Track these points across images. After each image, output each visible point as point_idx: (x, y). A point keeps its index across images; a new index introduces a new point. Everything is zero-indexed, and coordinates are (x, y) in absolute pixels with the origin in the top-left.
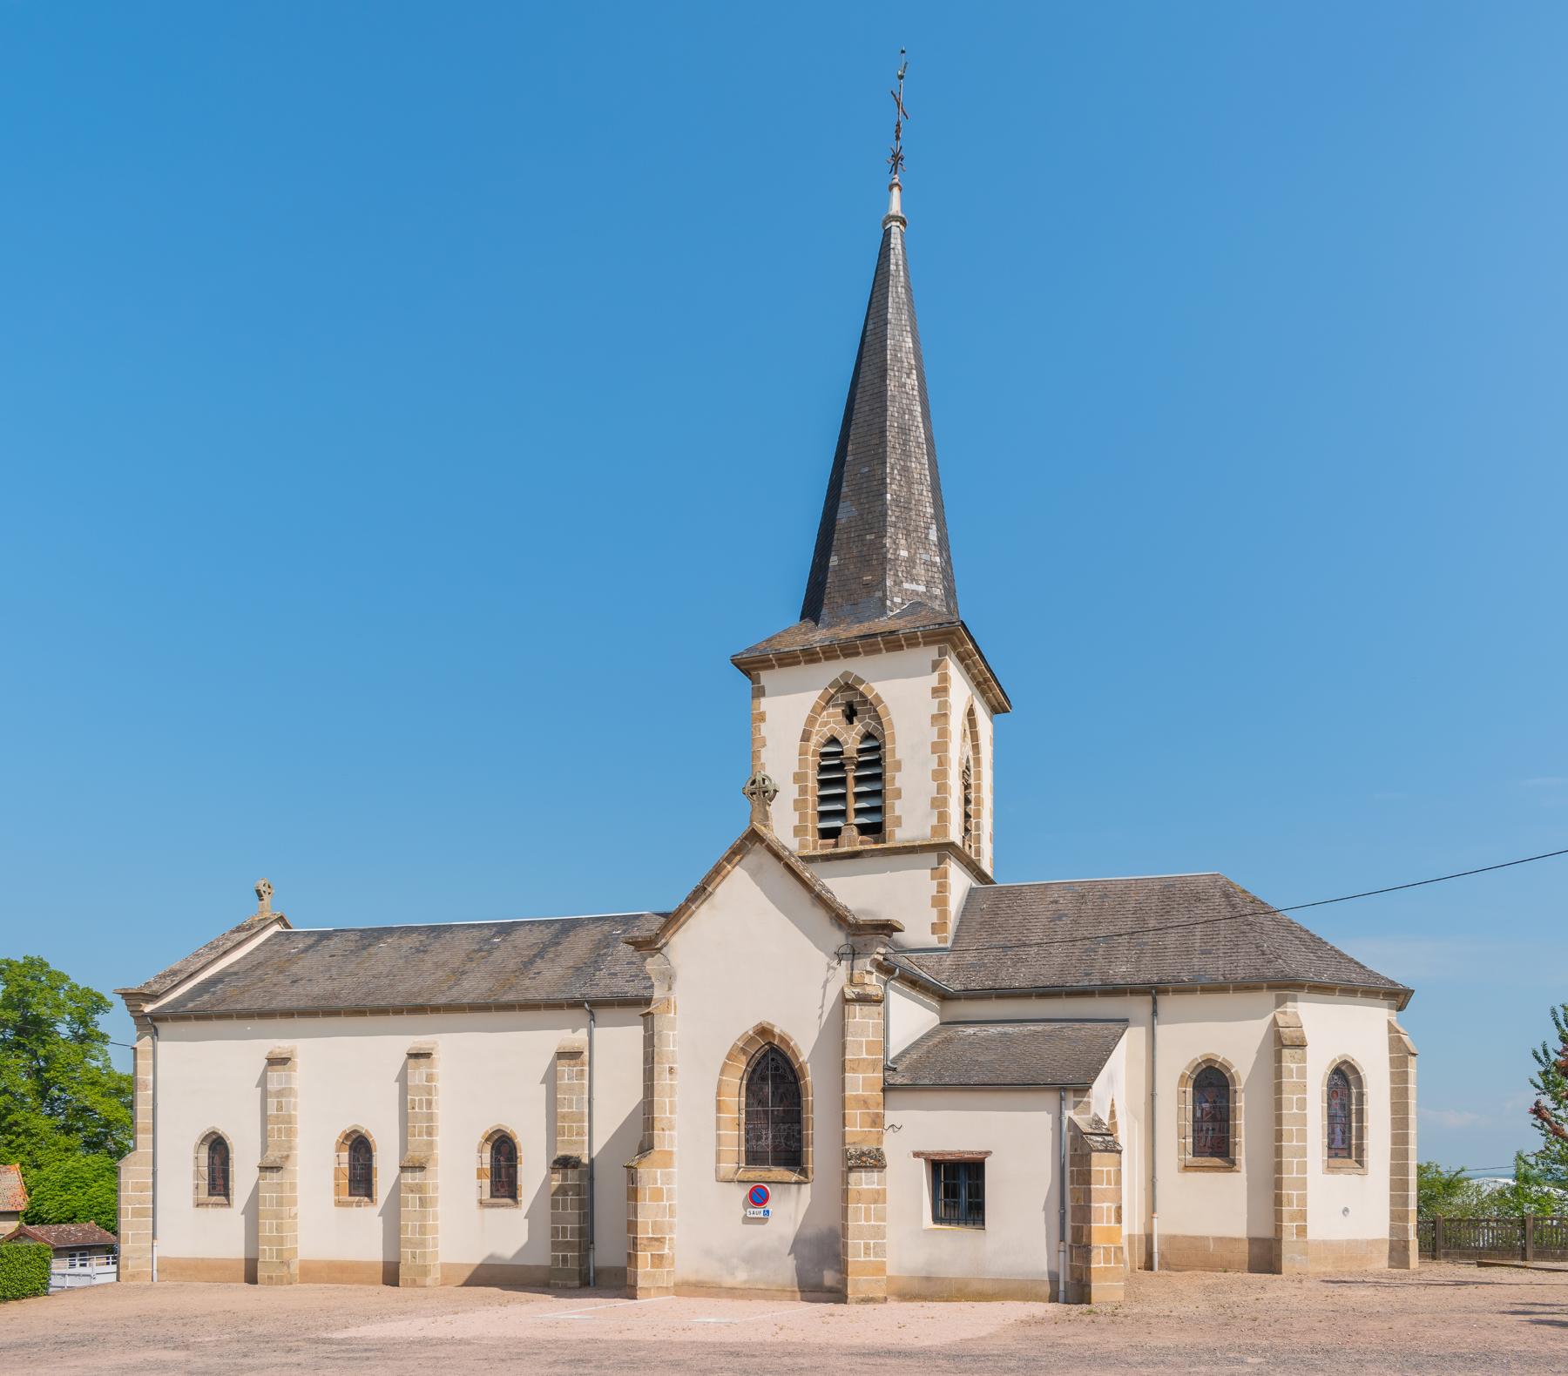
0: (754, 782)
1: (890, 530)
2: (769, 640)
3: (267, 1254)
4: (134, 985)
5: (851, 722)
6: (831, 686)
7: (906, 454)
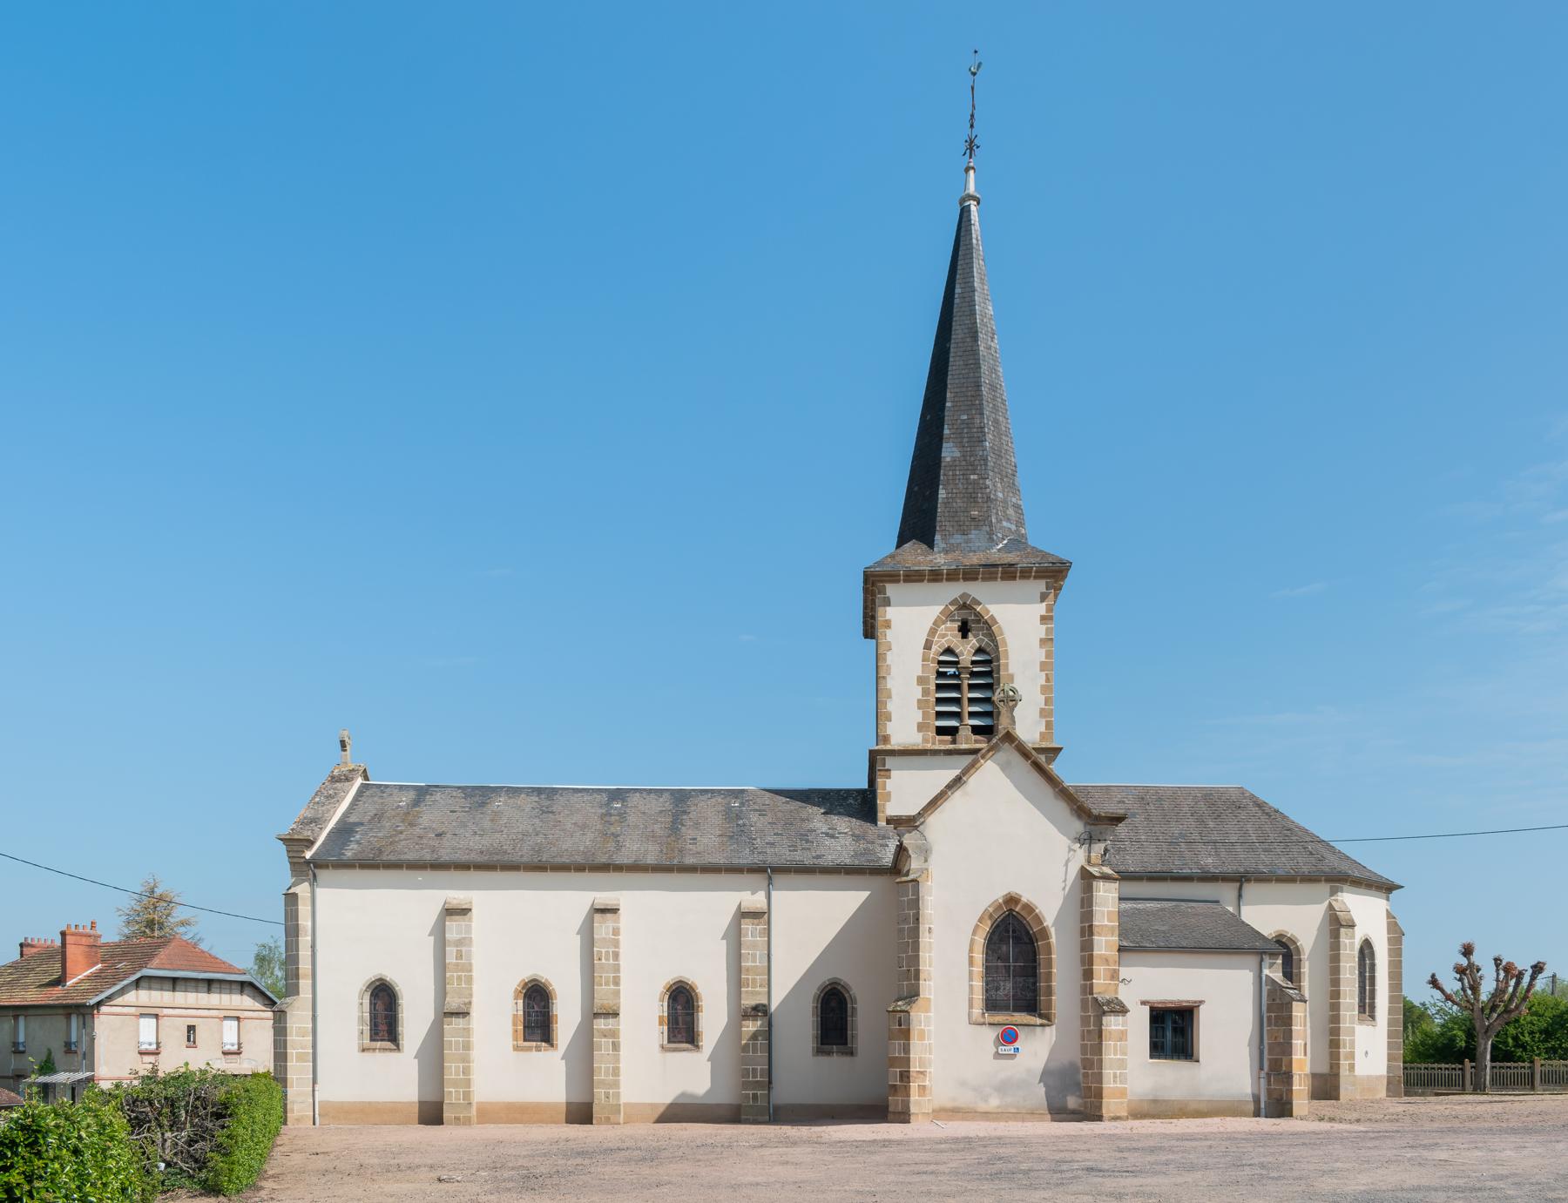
3: (452, 1095)
6: (951, 603)
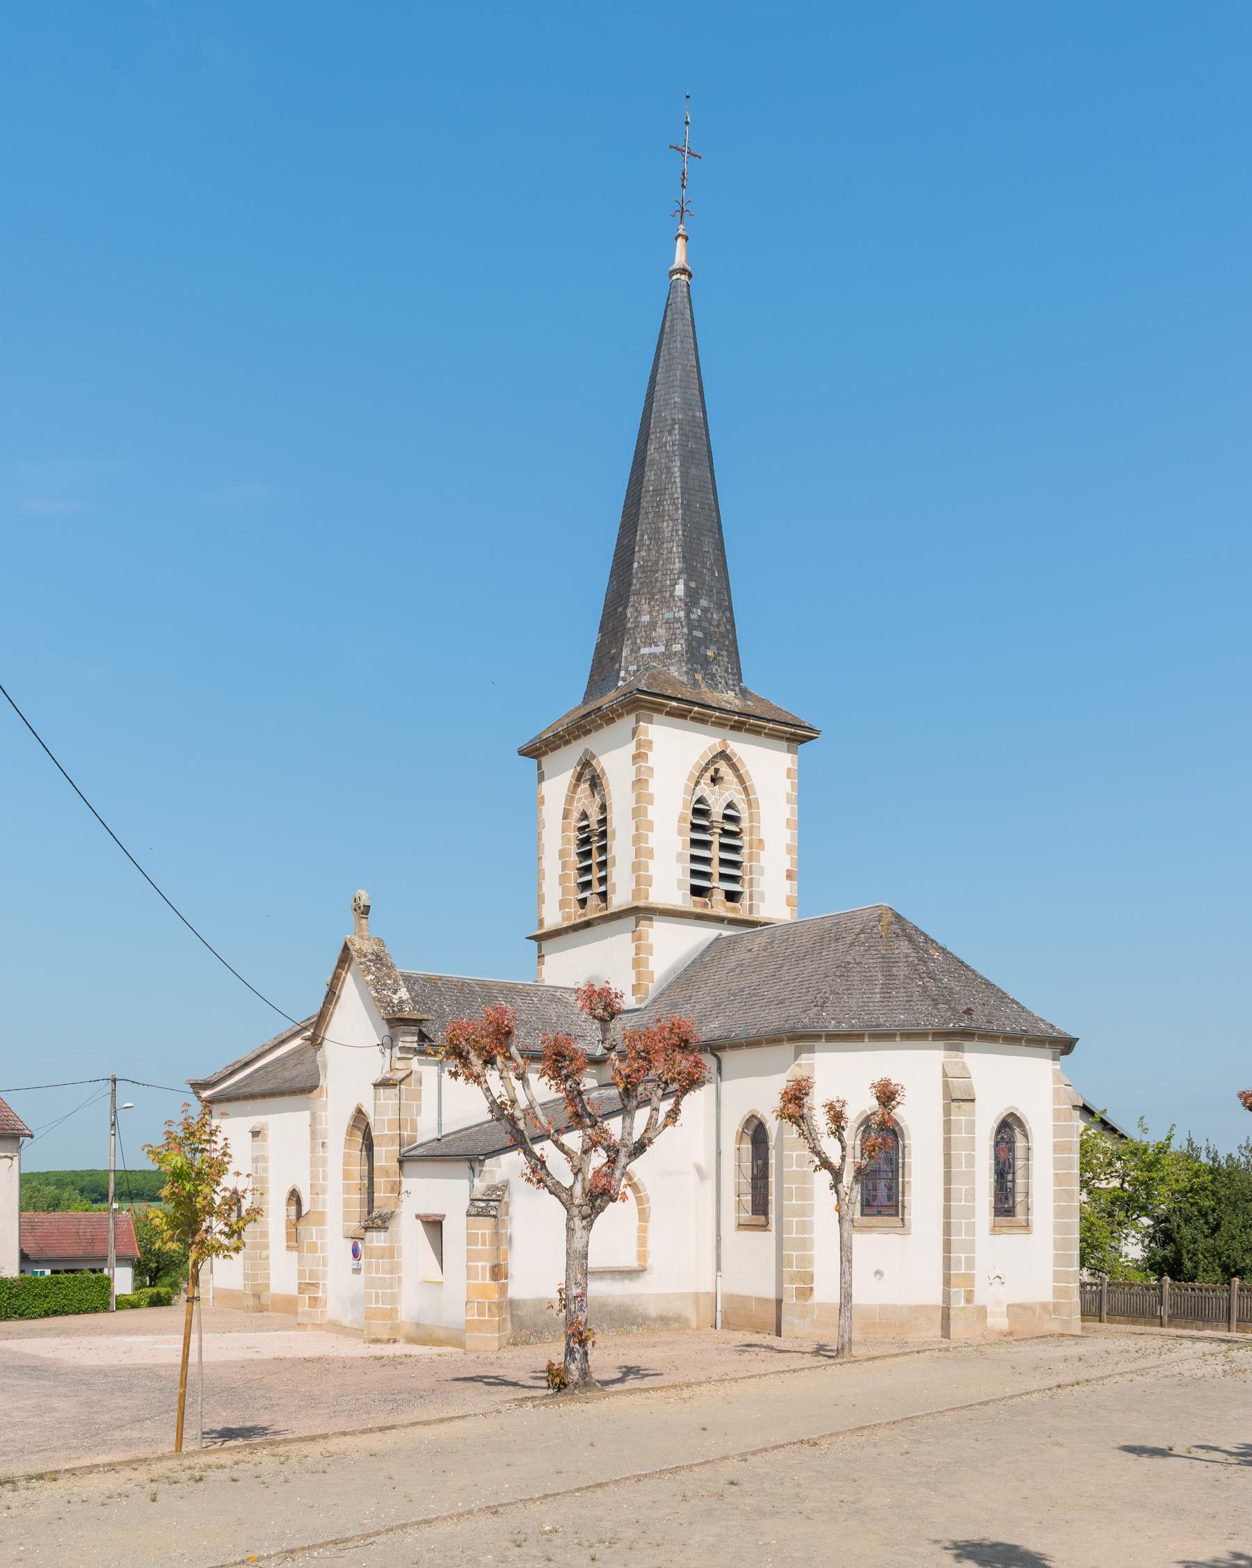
4: (201, 1077)
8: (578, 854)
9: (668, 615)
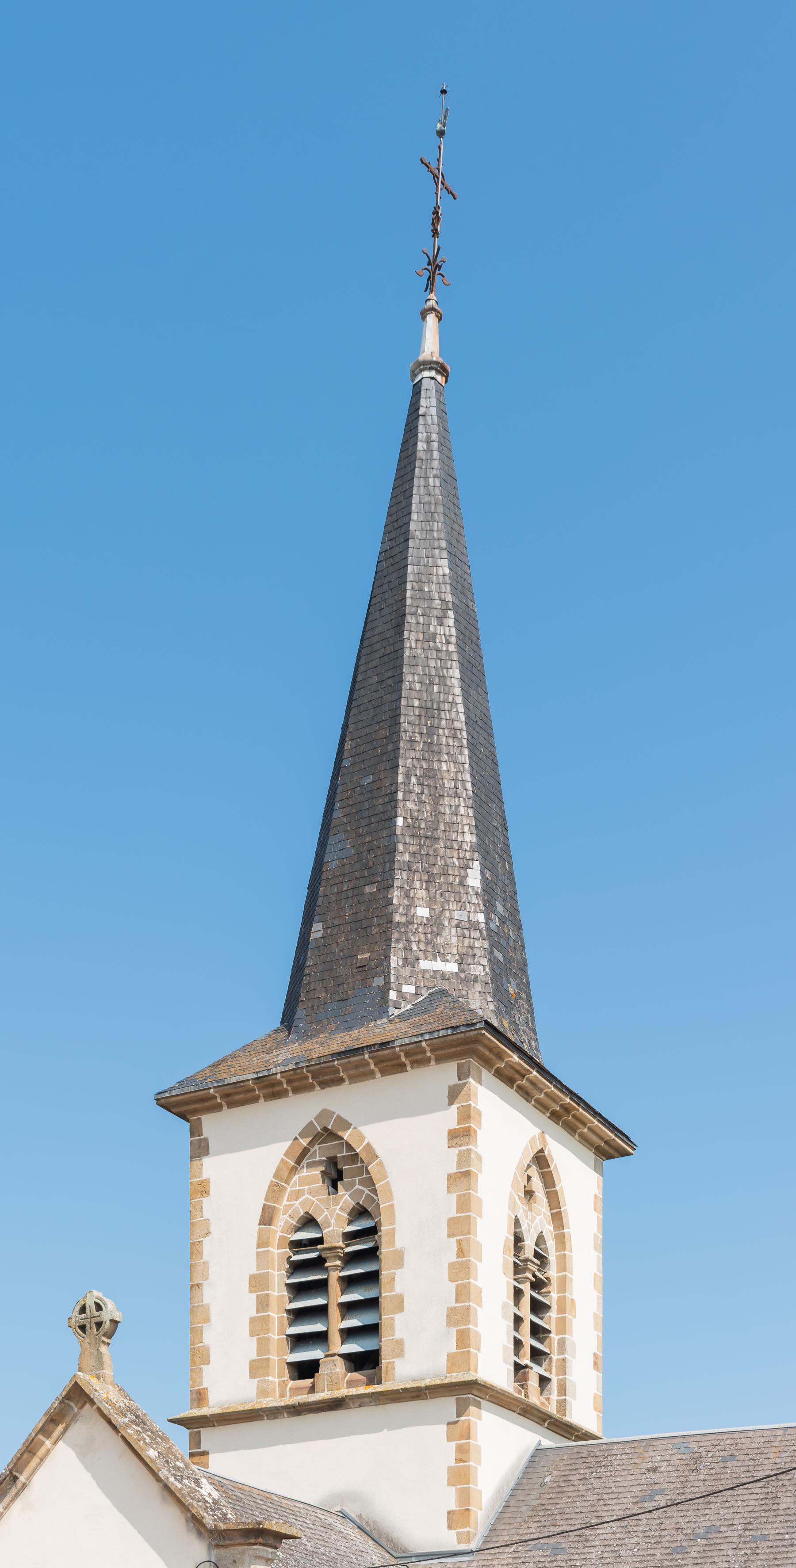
0: (83, 1310)
1: (400, 877)
2: (216, 1065)
5: (335, 1187)
6: (303, 1134)
7: (432, 750)
8: (290, 1286)
9: (460, 915)
